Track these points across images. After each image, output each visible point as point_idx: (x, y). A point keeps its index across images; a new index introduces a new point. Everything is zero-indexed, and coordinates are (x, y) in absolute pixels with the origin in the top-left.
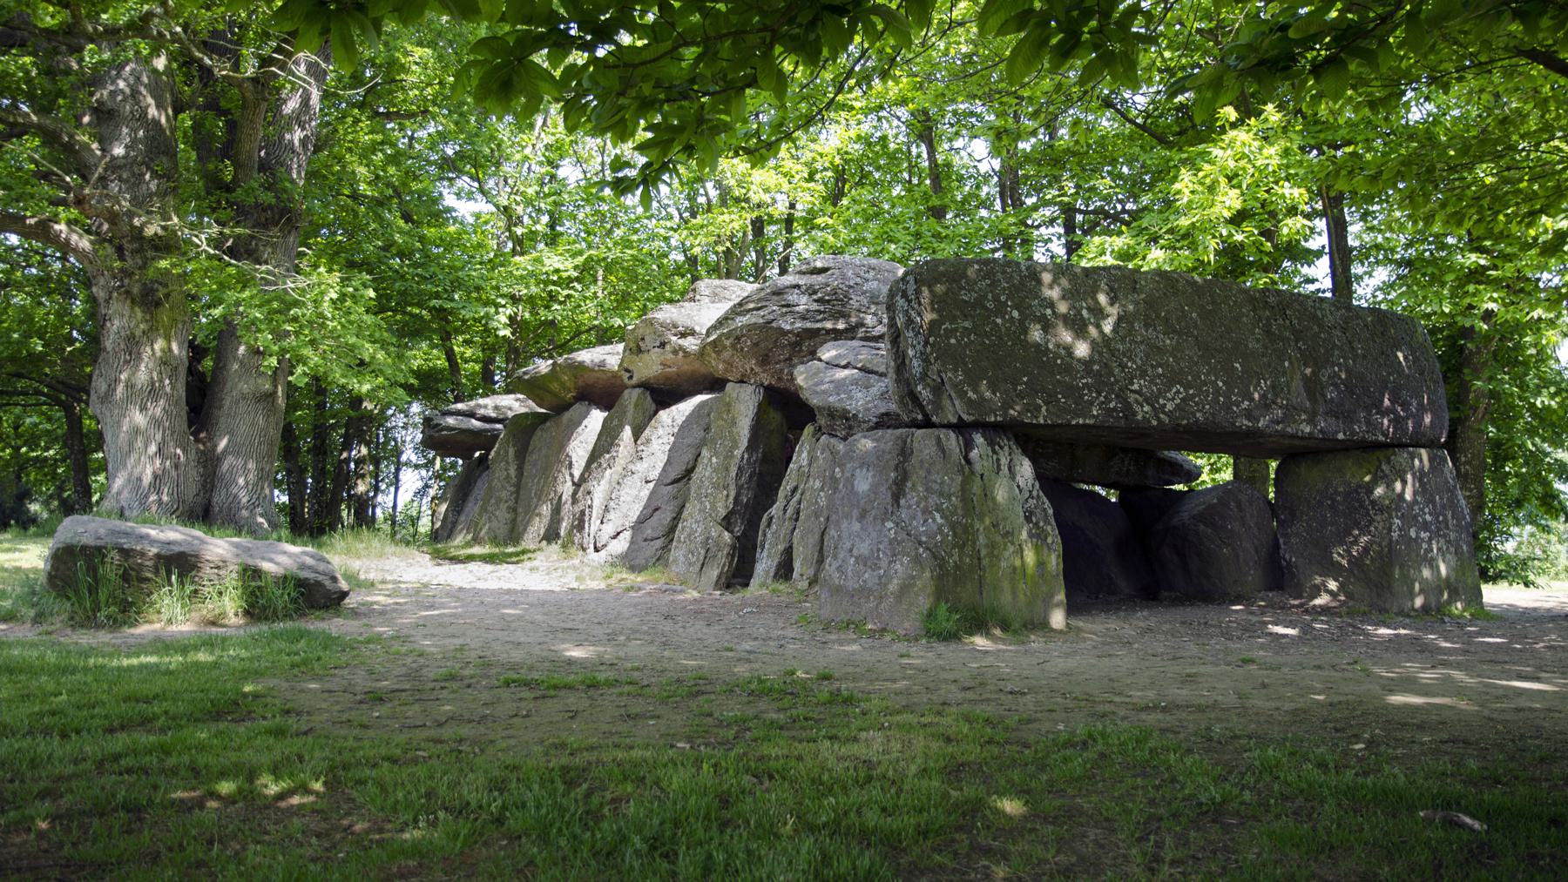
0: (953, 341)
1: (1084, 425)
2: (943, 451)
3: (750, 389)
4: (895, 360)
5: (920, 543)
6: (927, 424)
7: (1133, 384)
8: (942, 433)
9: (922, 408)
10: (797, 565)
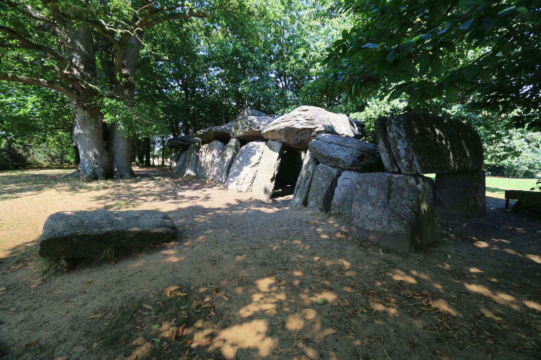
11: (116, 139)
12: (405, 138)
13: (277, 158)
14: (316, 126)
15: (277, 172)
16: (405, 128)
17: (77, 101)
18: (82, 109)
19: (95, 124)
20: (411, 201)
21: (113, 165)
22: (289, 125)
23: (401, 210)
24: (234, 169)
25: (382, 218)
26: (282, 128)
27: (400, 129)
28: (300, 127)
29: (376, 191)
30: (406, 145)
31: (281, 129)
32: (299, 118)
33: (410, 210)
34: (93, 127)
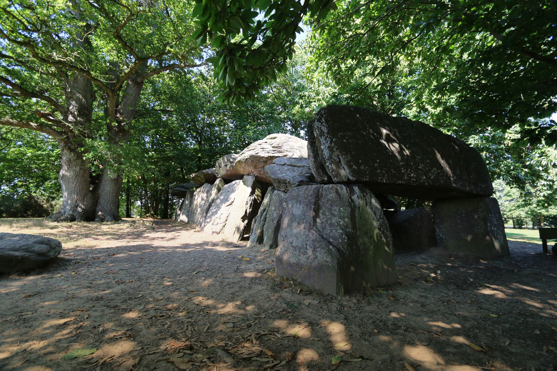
0: (345, 141)
1: (401, 184)
2: (339, 195)
3: (250, 177)
4: (313, 153)
5: (330, 243)
6: (330, 181)
7: (419, 166)
8: (338, 187)
9: (326, 174)
10: (265, 238)
11: (103, 181)
12: (328, 133)
13: (249, 194)
14: (285, 154)
15: (251, 210)
16: (326, 121)
17: (65, 143)
18: (69, 151)
19: (81, 166)
20: (343, 218)
21: (96, 208)
22: (254, 154)
23: (330, 232)
24: (213, 209)
25: (307, 244)
26: (247, 157)
27: (322, 123)
28: (266, 155)
29: (301, 209)
30: (329, 142)
31: (247, 159)
32: (265, 146)
33: (340, 231)
34: (78, 168)
